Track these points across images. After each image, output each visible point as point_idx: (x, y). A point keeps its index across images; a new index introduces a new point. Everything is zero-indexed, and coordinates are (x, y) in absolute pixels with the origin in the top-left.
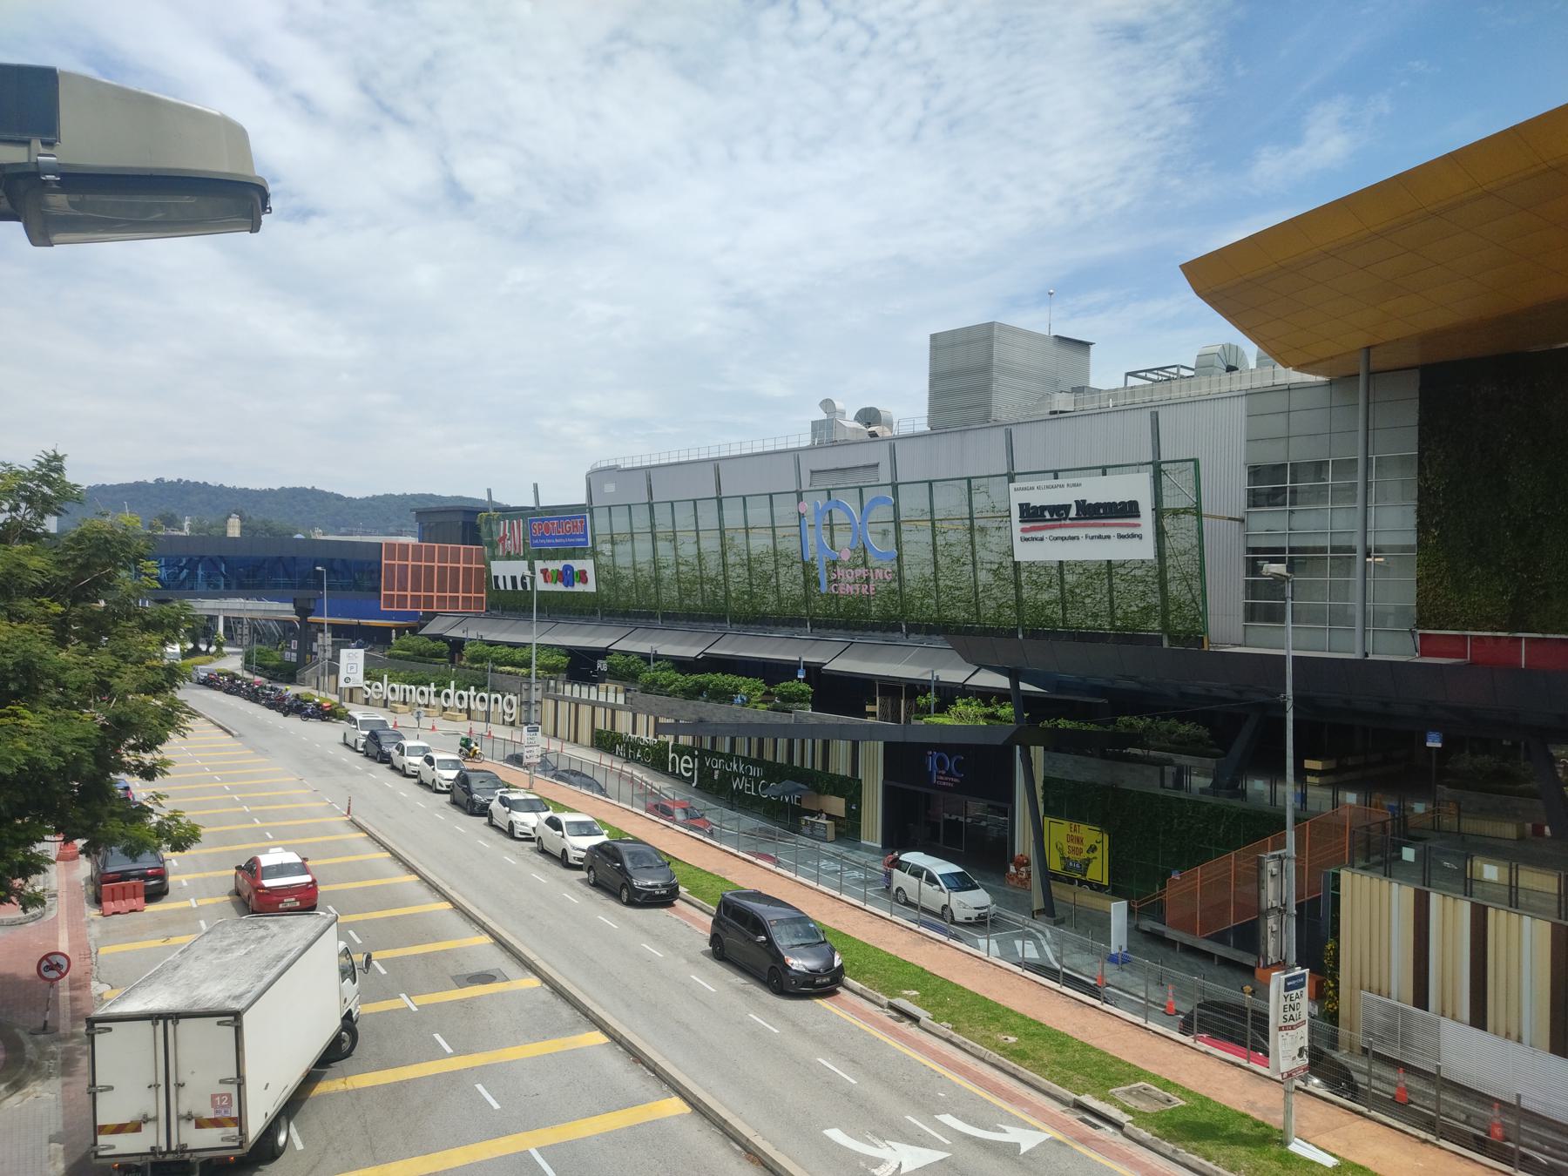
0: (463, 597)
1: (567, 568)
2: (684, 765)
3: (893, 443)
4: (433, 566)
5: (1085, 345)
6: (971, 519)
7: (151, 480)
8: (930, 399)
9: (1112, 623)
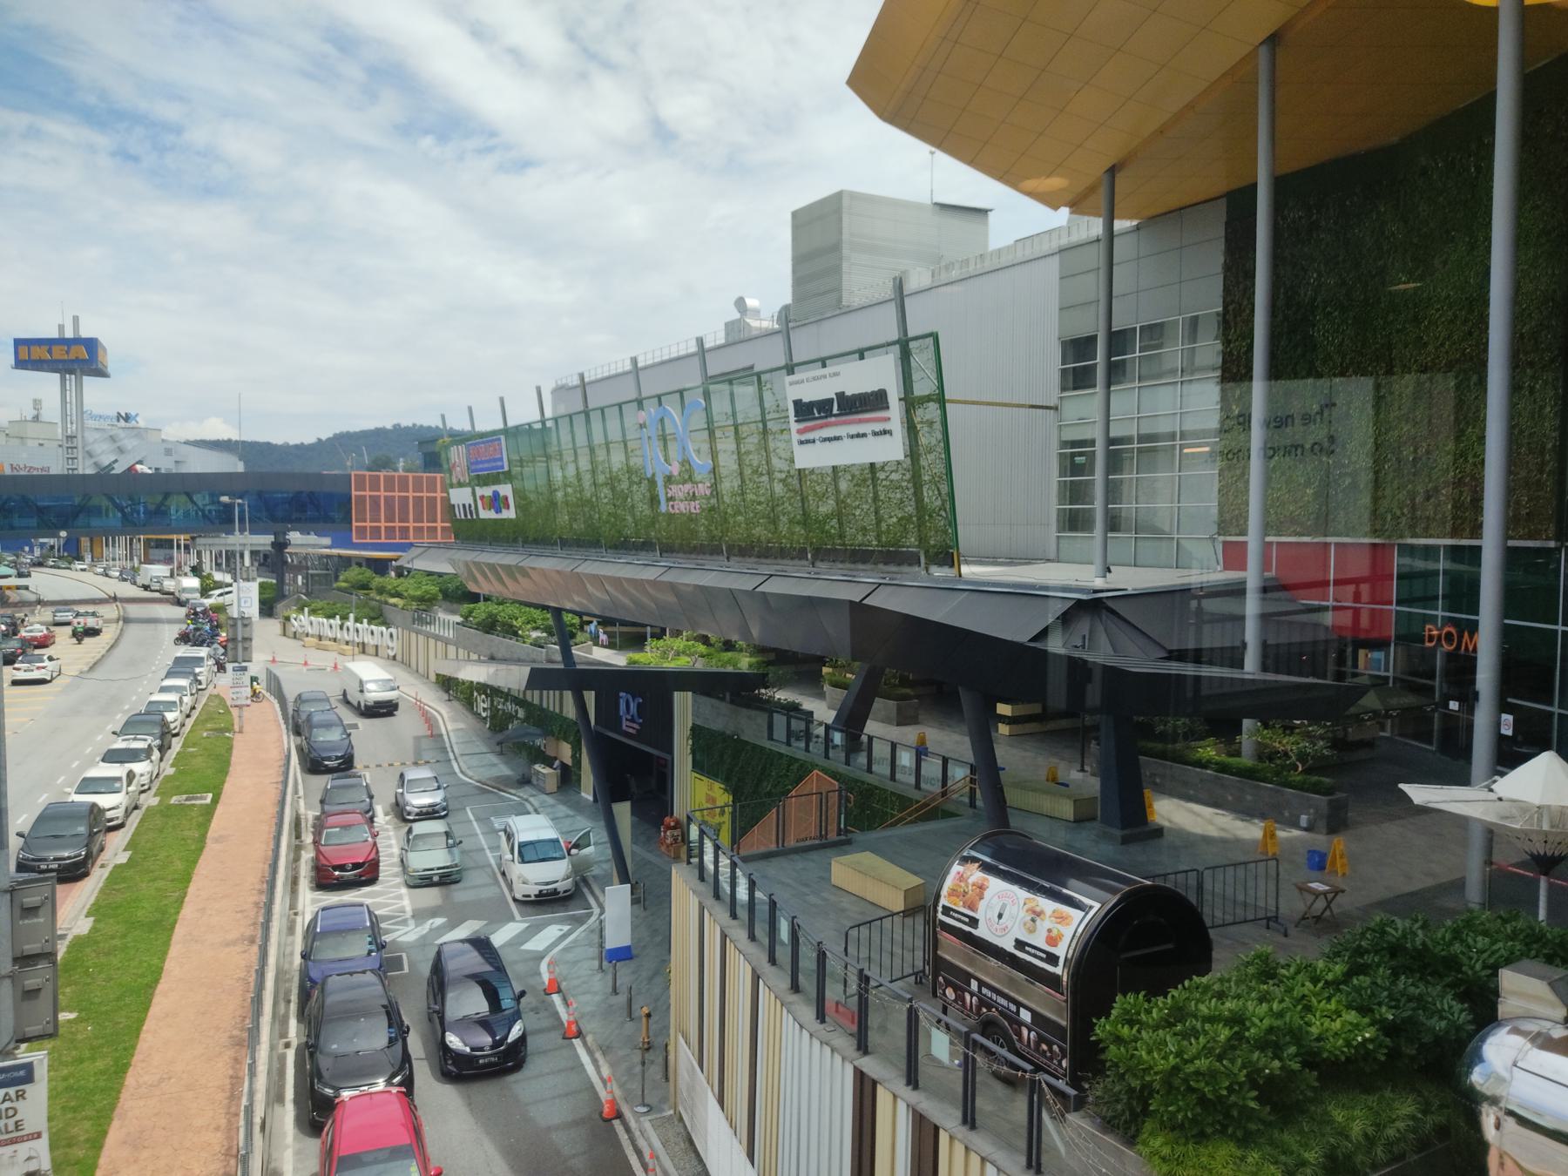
0: (386, 527)
2: (482, 704)
4: (408, 497)
5: (982, 212)
6: (764, 421)
7: (389, 426)
8: (793, 286)
9: (878, 537)
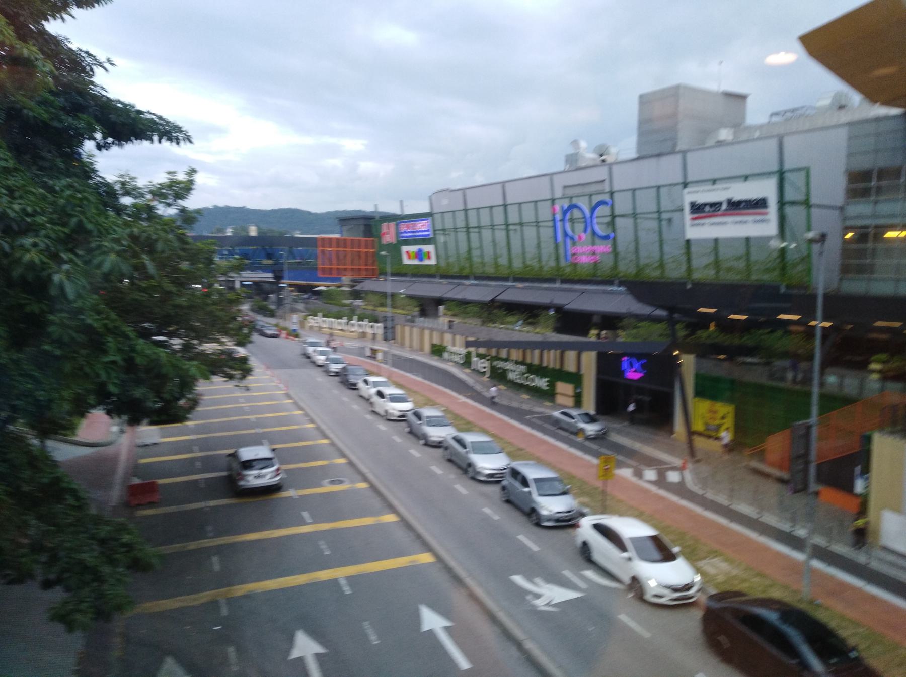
1: (420, 251)
3: (610, 165)
